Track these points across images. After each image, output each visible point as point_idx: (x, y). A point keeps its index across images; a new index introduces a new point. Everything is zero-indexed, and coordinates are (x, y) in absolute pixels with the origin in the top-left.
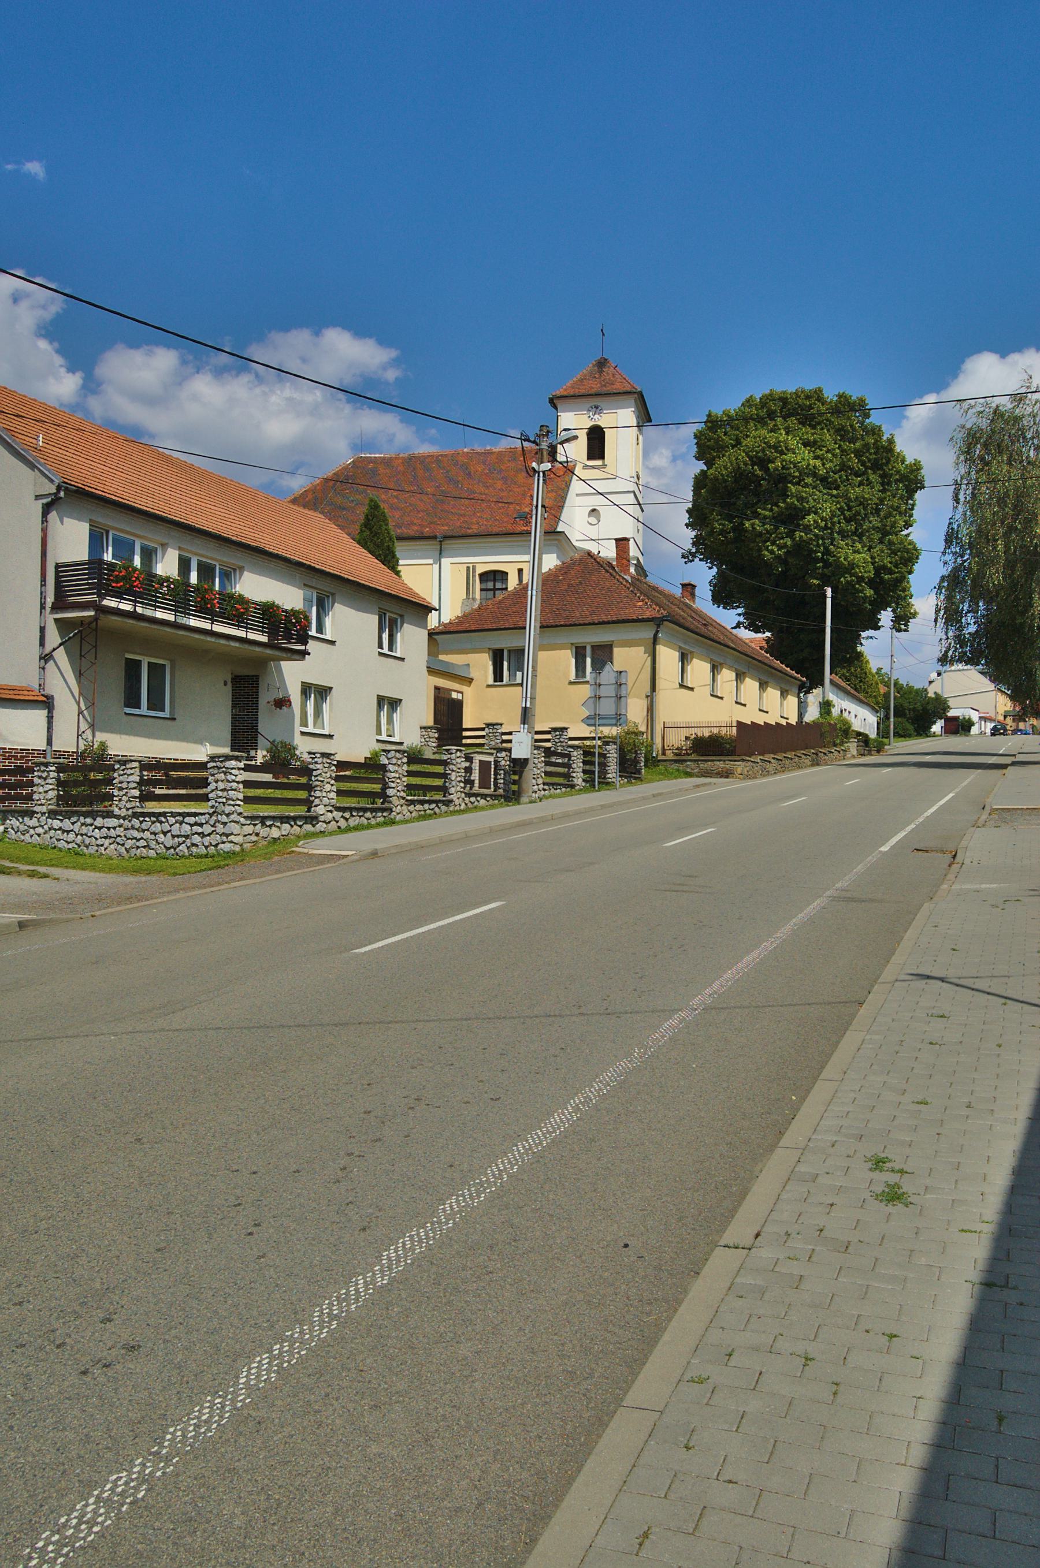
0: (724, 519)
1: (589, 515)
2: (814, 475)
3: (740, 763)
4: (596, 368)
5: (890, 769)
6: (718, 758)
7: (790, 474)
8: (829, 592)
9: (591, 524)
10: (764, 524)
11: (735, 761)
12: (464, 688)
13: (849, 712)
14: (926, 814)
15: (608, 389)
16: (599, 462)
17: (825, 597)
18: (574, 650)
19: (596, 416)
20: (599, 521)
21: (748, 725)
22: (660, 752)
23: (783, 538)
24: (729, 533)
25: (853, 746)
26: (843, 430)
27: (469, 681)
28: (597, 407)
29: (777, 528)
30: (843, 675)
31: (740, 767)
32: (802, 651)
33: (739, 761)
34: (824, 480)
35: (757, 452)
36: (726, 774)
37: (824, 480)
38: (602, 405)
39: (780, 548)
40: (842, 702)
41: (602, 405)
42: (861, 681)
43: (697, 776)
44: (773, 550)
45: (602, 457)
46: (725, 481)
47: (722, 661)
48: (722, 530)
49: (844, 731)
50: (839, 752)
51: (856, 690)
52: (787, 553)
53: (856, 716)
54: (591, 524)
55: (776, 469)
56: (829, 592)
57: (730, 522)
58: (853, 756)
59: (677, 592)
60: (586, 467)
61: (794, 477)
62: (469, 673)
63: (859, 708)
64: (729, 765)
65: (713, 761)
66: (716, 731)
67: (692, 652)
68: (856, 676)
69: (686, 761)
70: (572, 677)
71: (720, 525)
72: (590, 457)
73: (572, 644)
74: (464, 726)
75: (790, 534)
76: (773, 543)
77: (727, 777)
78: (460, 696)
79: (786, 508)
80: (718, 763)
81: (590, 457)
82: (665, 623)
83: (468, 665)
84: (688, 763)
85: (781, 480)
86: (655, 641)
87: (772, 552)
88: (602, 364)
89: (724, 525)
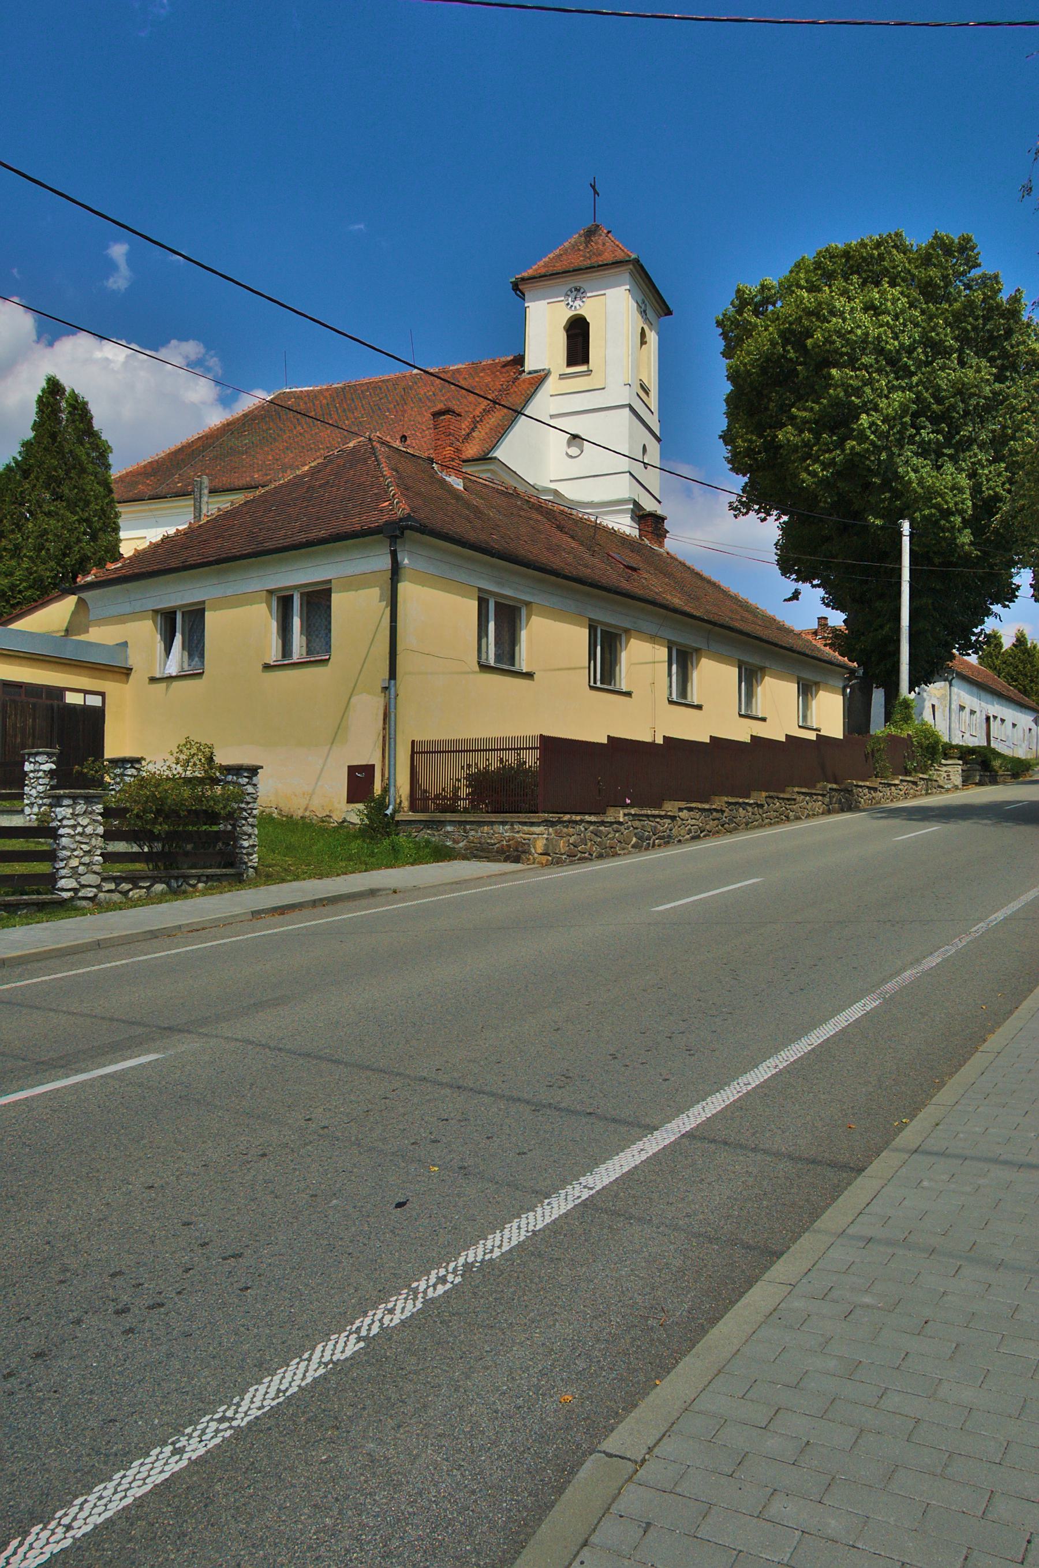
0: (752, 433)
1: (569, 444)
2: (880, 351)
3: (542, 829)
4: (583, 239)
5: (933, 828)
6: (500, 817)
7: (836, 351)
8: (906, 527)
9: (571, 457)
10: (801, 431)
11: (532, 824)
12: (108, 686)
13: (1003, 721)
14: (474, 1254)
15: (595, 260)
16: (584, 368)
17: (900, 535)
18: (274, 604)
19: (577, 303)
20: (582, 452)
21: (707, 743)
22: (406, 804)
23: (830, 451)
24: (759, 453)
25: (952, 771)
26: (930, 285)
27: (125, 672)
28: (577, 290)
29: (818, 436)
30: (1009, 674)
31: (539, 837)
32: (882, 627)
33: (538, 824)
34: (893, 361)
35: (791, 324)
36: (515, 853)
37: (893, 361)
38: (584, 285)
39: (825, 466)
40: (990, 707)
41: (584, 285)
42: (1032, 681)
43: (465, 858)
44: (814, 471)
45: (585, 360)
46: (748, 373)
47: (627, 625)
48: (748, 449)
49: (927, 748)
50: (915, 783)
51: (1025, 692)
52: (838, 474)
53: (1014, 725)
54: (571, 457)
55: (816, 345)
56: (906, 527)
57: (760, 436)
58: (956, 787)
59: (624, 524)
60: (563, 377)
61: (842, 354)
62: (127, 658)
63: (1019, 714)
64: (521, 834)
65: (492, 823)
66: (511, 758)
67: (528, 604)
68: (1026, 675)
69: (443, 823)
70: (273, 653)
71: (744, 441)
72: (571, 362)
73: (270, 592)
74: (986, 744)
75: (840, 444)
76: (816, 460)
77: (517, 860)
78: (94, 701)
79: (831, 406)
80: (501, 829)
81: (571, 362)
82: (407, 532)
83: (126, 643)
84: (449, 828)
85: (825, 360)
86: (396, 572)
87: (814, 474)
88: (591, 233)
89: (750, 441)
